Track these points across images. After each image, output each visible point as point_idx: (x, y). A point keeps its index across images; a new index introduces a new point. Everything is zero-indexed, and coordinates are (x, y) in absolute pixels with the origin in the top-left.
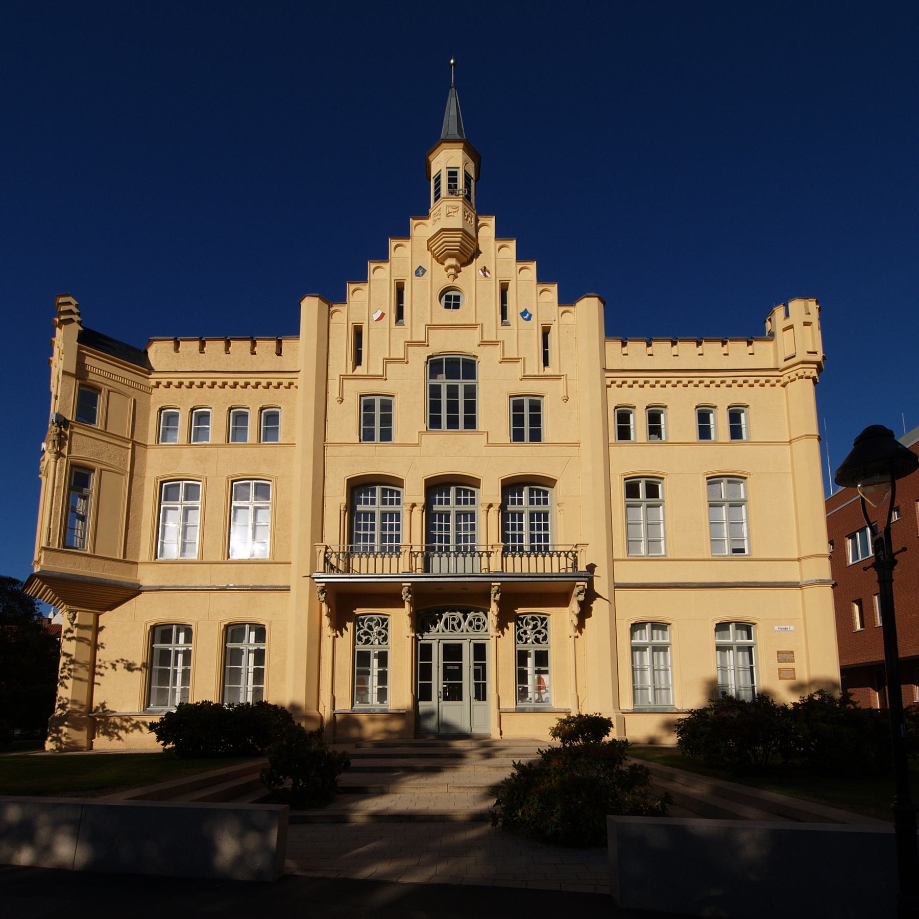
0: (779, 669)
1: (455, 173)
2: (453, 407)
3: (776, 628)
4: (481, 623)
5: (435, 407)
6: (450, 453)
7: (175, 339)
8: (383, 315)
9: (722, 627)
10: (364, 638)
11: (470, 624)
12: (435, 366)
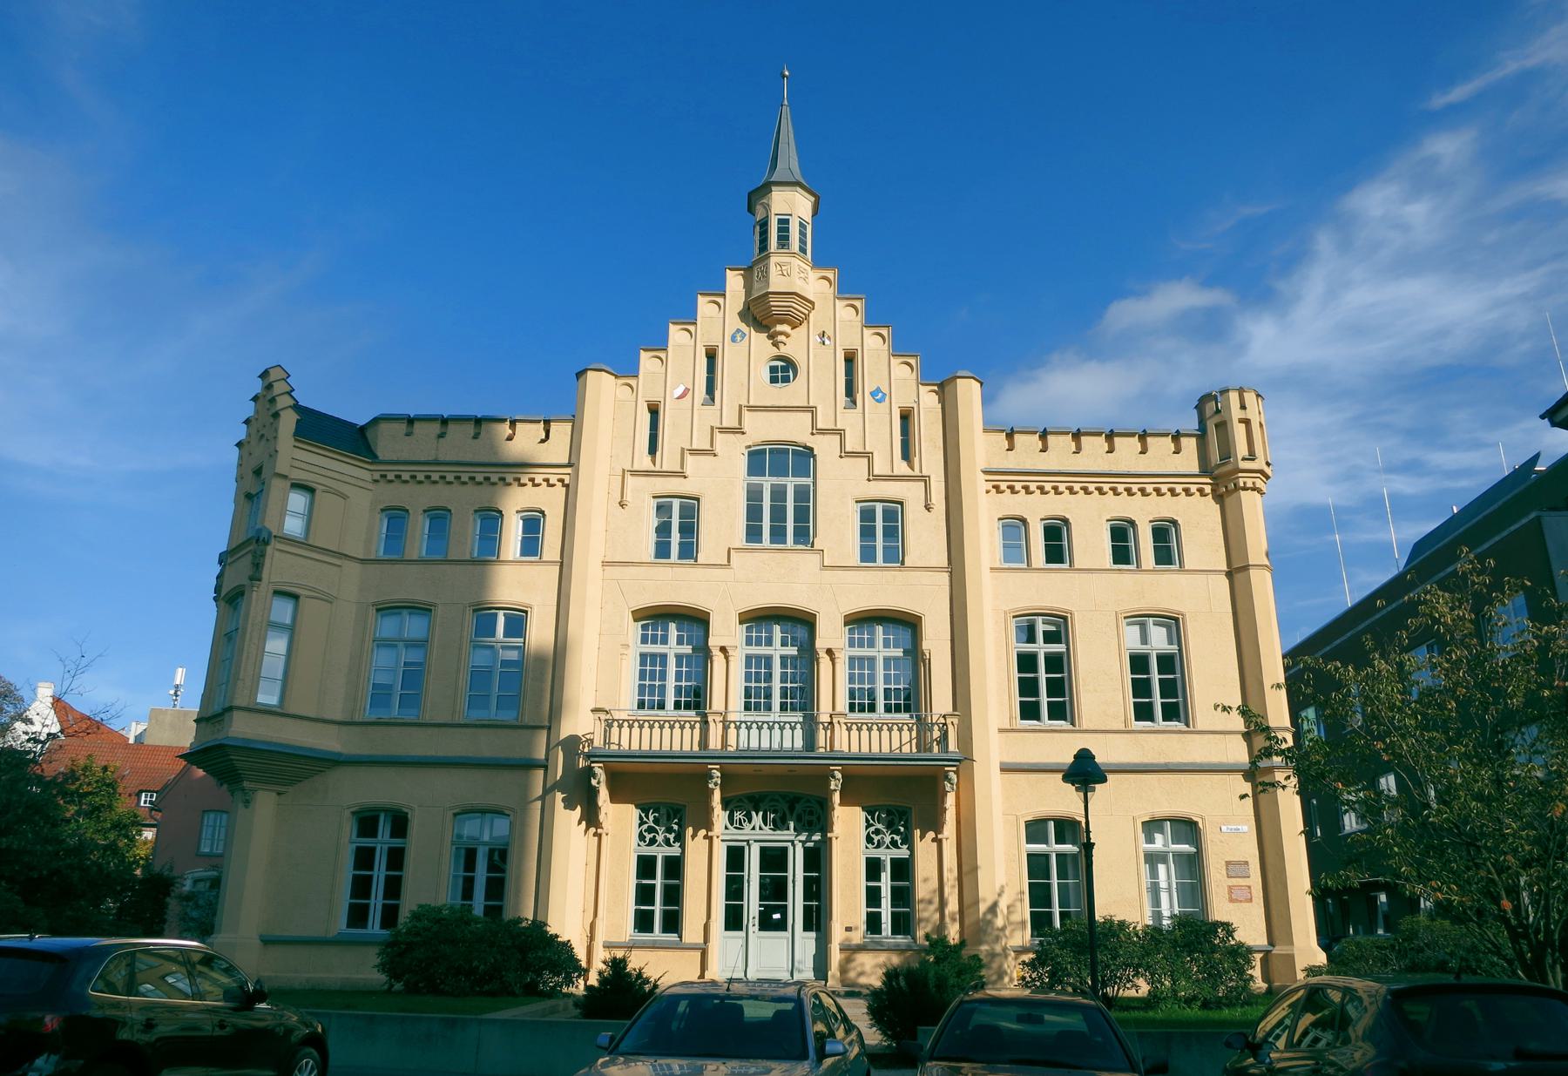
0: (1230, 887)
1: (787, 221)
2: (778, 514)
4: (814, 818)
5: (754, 513)
6: (783, 578)
7: (547, 423)
8: (687, 390)
9: (1152, 827)
10: (648, 836)
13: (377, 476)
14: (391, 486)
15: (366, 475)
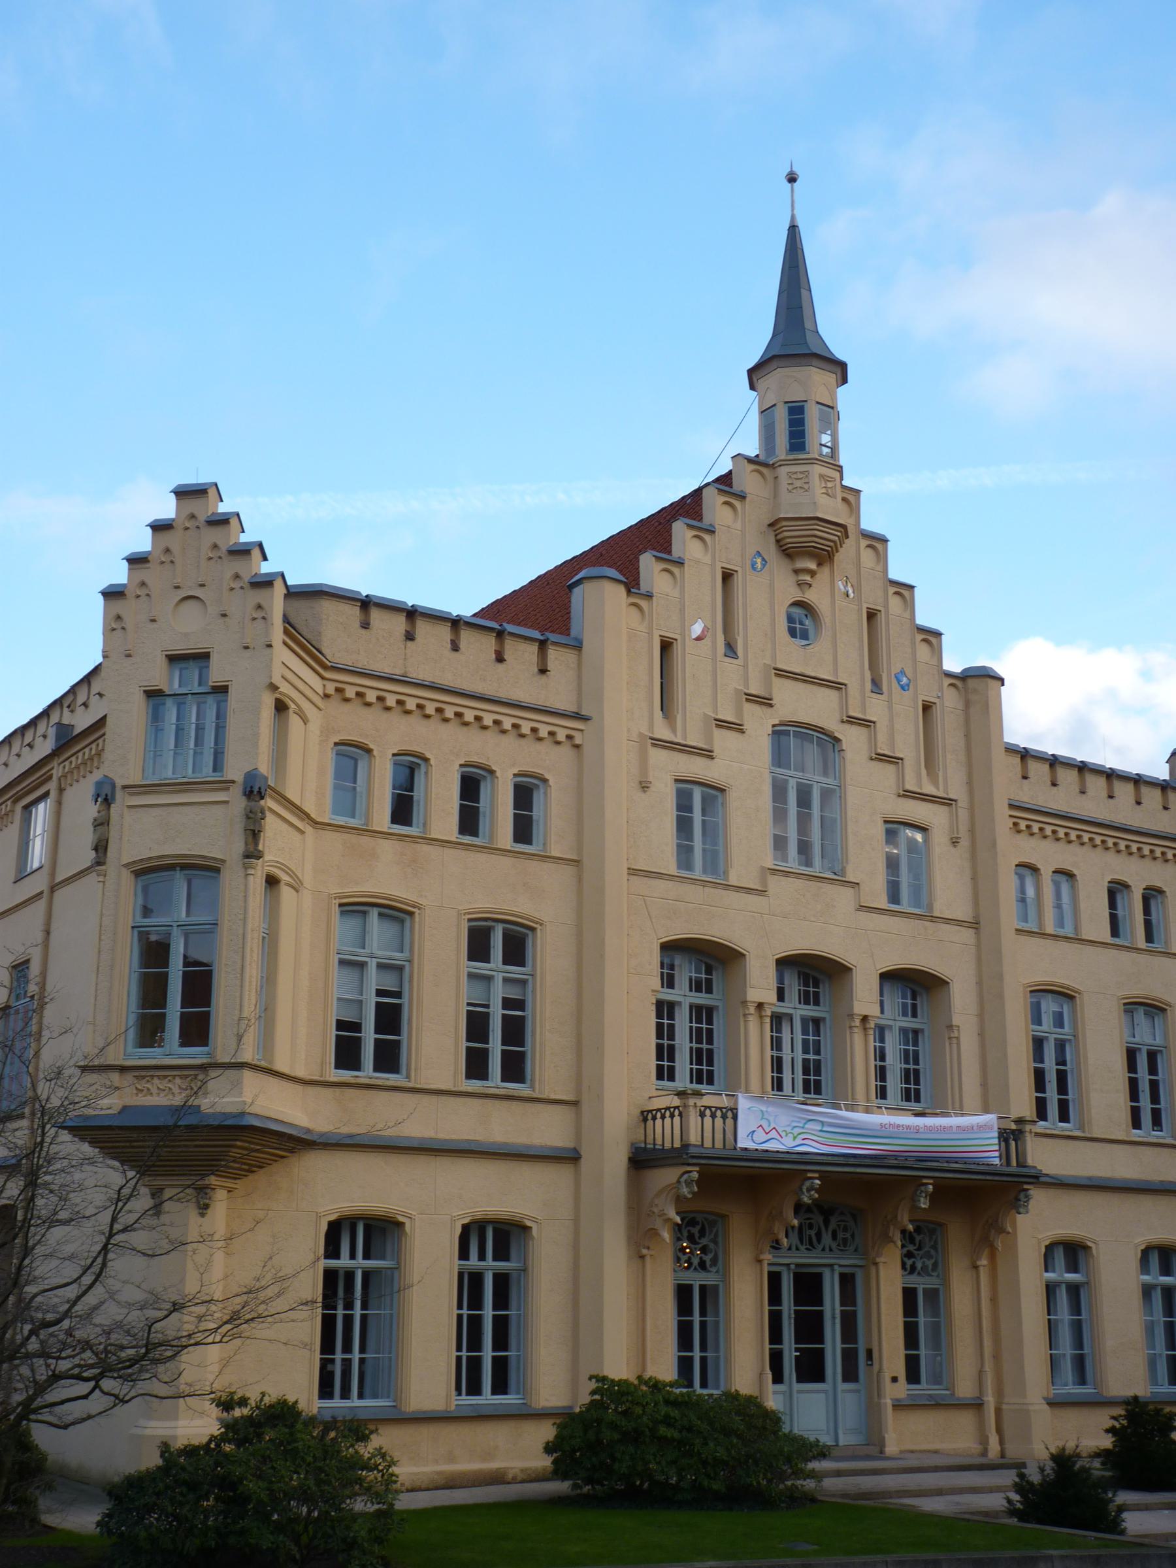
10: (909, 1262)
11: (834, 1237)
13: (330, 689)
14: (347, 707)
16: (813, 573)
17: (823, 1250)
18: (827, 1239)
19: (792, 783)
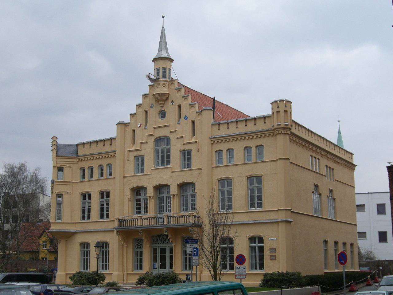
0: (270, 256)
3: (270, 239)
8: (141, 125)
10: (137, 246)
12: (157, 140)
15: (75, 160)
16: (163, 104)
17: (166, 243)
18: (159, 241)
19: (160, 150)
